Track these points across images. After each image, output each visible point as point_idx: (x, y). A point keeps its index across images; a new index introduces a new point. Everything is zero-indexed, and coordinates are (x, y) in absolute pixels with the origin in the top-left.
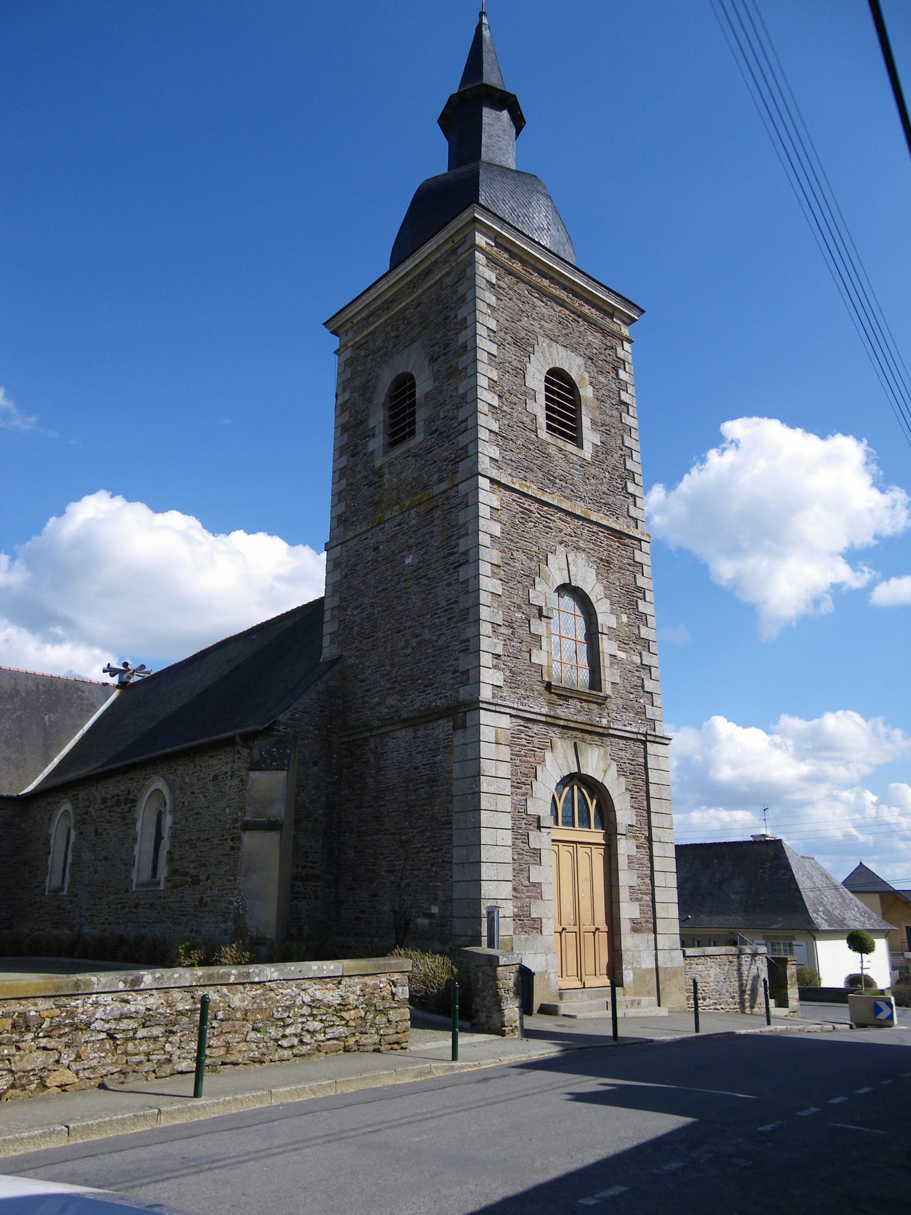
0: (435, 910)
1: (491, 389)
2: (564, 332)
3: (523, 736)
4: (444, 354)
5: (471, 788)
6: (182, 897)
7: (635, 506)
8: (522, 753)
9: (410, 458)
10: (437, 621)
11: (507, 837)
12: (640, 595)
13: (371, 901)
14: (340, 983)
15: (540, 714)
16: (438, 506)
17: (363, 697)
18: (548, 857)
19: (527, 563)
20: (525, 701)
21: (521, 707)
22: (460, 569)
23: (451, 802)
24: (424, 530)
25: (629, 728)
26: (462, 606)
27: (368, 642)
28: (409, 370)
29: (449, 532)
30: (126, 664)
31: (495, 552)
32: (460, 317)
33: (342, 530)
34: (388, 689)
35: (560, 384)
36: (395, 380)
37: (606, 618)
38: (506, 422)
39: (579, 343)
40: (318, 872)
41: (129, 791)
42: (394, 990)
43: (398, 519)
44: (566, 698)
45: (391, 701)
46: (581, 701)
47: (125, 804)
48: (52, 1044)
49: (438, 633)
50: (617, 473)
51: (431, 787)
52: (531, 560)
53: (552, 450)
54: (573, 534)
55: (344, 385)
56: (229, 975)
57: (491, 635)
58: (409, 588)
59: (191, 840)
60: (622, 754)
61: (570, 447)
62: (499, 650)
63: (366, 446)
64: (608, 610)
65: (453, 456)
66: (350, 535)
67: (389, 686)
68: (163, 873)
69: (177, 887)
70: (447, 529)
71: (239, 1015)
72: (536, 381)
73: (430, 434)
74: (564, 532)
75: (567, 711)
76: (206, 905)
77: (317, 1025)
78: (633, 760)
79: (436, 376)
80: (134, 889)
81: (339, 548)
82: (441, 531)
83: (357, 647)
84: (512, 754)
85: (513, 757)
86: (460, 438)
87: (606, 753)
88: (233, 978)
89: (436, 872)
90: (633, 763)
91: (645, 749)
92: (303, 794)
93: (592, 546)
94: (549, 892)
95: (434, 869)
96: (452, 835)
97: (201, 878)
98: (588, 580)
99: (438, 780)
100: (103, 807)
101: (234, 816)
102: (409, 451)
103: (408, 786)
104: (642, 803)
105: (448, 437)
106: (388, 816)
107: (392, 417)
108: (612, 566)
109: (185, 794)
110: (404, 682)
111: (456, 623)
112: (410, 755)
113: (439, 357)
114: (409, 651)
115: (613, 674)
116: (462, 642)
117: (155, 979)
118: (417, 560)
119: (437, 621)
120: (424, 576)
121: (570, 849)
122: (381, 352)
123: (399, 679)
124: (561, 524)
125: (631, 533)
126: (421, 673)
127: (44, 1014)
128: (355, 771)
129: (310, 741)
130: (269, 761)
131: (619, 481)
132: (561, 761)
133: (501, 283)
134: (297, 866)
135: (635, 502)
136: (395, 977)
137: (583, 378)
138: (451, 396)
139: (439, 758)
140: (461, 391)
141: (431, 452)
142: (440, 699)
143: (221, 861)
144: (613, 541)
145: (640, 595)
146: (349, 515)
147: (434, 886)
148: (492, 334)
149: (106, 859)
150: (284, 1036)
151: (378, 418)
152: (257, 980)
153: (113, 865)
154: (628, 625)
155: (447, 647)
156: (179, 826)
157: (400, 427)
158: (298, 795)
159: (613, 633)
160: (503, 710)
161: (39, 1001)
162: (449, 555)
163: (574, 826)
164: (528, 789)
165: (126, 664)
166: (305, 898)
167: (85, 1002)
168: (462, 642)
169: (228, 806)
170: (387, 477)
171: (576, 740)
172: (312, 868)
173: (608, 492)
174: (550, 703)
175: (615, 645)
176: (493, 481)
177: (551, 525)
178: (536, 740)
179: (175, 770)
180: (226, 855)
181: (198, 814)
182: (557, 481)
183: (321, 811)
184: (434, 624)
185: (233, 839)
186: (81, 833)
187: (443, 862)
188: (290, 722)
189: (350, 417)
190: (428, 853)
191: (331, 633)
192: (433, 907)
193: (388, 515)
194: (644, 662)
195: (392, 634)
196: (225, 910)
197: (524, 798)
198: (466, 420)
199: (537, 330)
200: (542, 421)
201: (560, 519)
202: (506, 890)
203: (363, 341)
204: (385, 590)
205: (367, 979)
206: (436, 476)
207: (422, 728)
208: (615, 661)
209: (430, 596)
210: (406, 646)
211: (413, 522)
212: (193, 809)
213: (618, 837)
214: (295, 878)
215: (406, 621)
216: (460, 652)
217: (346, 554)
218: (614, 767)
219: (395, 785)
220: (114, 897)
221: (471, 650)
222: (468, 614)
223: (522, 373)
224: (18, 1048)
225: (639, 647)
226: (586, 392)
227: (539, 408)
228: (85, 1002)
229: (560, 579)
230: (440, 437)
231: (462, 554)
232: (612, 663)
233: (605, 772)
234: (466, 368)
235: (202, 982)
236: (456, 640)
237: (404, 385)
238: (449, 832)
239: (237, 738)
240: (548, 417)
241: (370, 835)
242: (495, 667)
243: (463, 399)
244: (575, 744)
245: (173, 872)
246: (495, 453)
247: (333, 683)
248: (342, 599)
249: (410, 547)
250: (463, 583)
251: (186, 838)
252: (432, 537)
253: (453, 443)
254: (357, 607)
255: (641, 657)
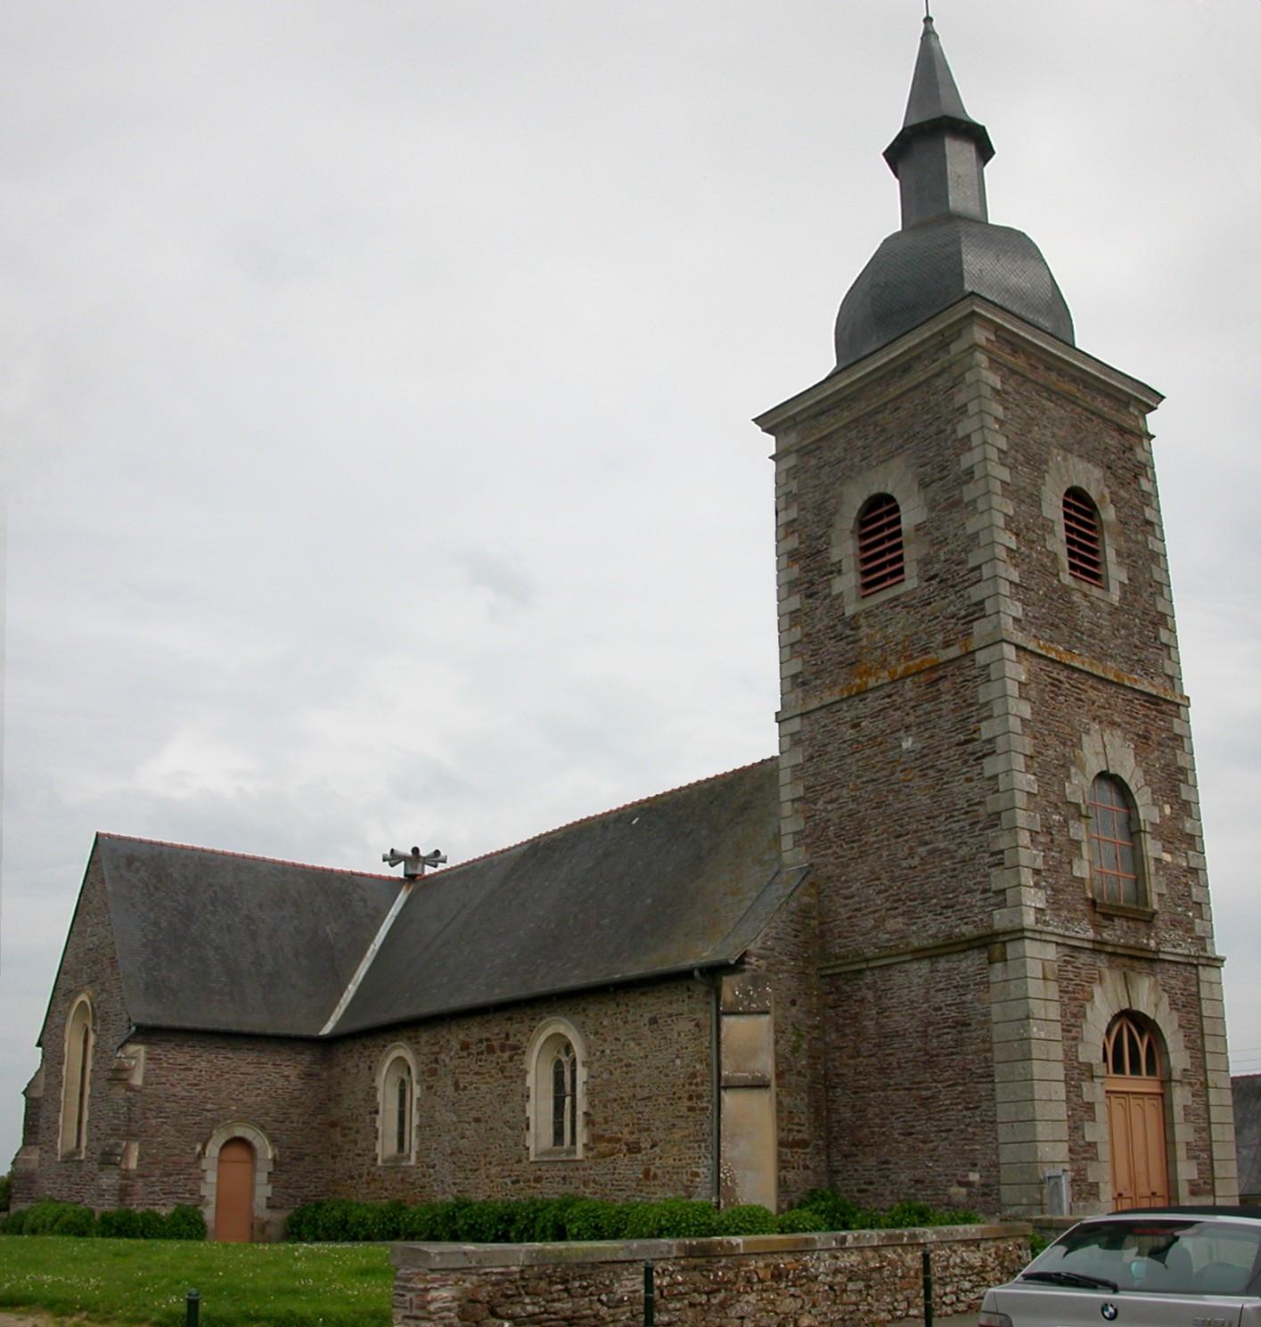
0: (974, 1177)
1: (1007, 527)
2: (1079, 437)
3: (1069, 968)
4: (941, 479)
5: (1018, 1034)
6: (615, 1168)
7: (1170, 658)
8: (1070, 989)
9: (898, 609)
10: (955, 826)
11: (1060, 1091)
12: (1181, 777)
13: (881, 1170)
14: (978, 1246)
15: (1083, 939)
16: (946, 676)
17: (850, 918)
18: (1100, 1111)
19: (1060, 748)
20: (1069, 925)
21: (1067, 933)
22: (984, 761)
23: (990, 1050)
24: (928, 707)
25: (1179, 951)
26: (990, 809)
27: (853, 848)
28: (889, 491)
29: (965, 712)
30: (415, 850)
31: (1027, 740)
32: (960, 434)
33: (800, 695)
34: (888, 910)
35: (1078, 501)
36: (866, 502)
37: (1148, 813)
38: (1025, 567)
39: (1095, 449)
40: (806, 1136)
41: (507, 1035)
42: (1020, 1253)
43: (887, 690)
44: (1109, 917)
45: (891, 924)
46: (1128, 919)
47: (503, 1051)
48: (798, 1291)
49: (959, 840)
50: (1149, 618)
51: (960, 1032)
52: (1064, 744)
53: (1076, 597)
54: (1107, 706)
55: (785, 498)
56: (902, 1236)
57: (1029, 845)
58: (910, 780)
59: (622, 1098)
60: (1172, 982)
61: (1096, 592)
62: (1039, 864)
63: (828, 584)
64: (1150, 802)
65: (963, 613)
66: (815, 704)
67: (888, 905)
68: (413, 1141)
69: (605, 1157)
70: (962, 708)
71: (912, 1273)
72: (1053, 509)
73: (927, 580)
74: (1097, 704)
75: (1114, 934)
76: (838, 1172)
77: (967, 1285)
78: (1185, 990)
79: (932, 506)
80: (532, 1159)
81: (798, 720)
82: (953, 710)
83: (835, 853)
84: (1061, 991)
85: (1062, 994)
86: (971, 590)
87: (1156, 981)
88: (905, 1239)
89: (974, 1134)
90: (1185, 993)
91: (1197, 974)
92: (782, 1042)
93: (1128, 719)
94: (1103, 1152)
95: (970, 1130)
96: (994, 1090)
97: (643, 1146)
98: (1127, 767)
99: (970, 1025)
100: (465, 1054)
101: (691, 1070)
102: (896, 598)
103: (925, 1031)
104: (1195, 1041)
105: (953, 586)
106: (900, 1068)
107: (864, 549)
108: (1150, 743)
109: (605, 1040)
110: (911, 900)
111: (983, 829)
112: (928, 992)
113: (933, 482)
114: (916, 861)
115: (1160, 883)
116: (993, 854)
117: (856, 1239)
118: (919, 746)
119: (955, 826)
120: (932, 767)
121: (1122, 1101)
122: (843, 464)
123: (903, 897)
124: (1093, 694)
125: (1168, 698)
126: (936, 890)
127: (789, 1267)
128: (845, 1011)
129: (786, 975)
130: (746, 1003)
131: (1151, 628)
132: (1110, 995)
133: (1006, 387)
134: (783, 1130)
135: (1169, 654)
136: (1021, 1240)
137: (1103, 496)
138: (956, 535)
139: (970, 997)
140: (970, 531)
141: (930, 603)
142: (966, 924)
143: (674, 1125)
144: (1149, 708)
145: (1181, 777)
146: (808, 676)
147: (972, 1150)
148: (1002, 456)
149: (477, 1120)
150: (946, 1294)
151: (845, 549)
152: (922, 1241)
153: (491, 1129)
154: (1171, 819)
155: (971, 860)
156: (598, 1081)
157: (880, 565)
158: (776, 1042)
159: (1158, 832)
160: (1048, 938)
161: (785, 1256)
162: (967, 742)
163: (1123, 1073)
164: (1078, 1032)
165: (415, 850)
166: (793, 1168)
167: (812, 1258)
168: (993, 854)
169: (678, 1057)
170: (864, 630)
171: (1125, 969)
172: (799, 1131)
173: (1141, 646)
174: (1095, 926)
175: (1159, 845)
176: (1018, 647)
177: (1083, 697)
178: (1083, 972)
179: (584, 1010)
180: (682, 1117)
181: (628, 1065)
182: (1085, 637)
183: (804, 1062)
184: (950, 829)
185: (690, 1098)
186: (429, 1088)
187: (983, 1121)
188: (762, 952)
189: (801, 543)
190: (961, 1111)
191: (795, 833)
192: (971, 1174)
193: (872, 683)
194: (1191, 865)
195: (888, 839)
196: (689, 1183)
197: (1074, 1043)
198: (979, 567)
199: (1049, 439)
200: (1064, 560)
201: (1092, 687)
202: (1062, 1151)
203: (812, 447)
204: (873, 780)
205: (998, 1243)
206: (940, 637)
207: (942, 960)
208: (1160, 865)
209: (943, 792)
210: (911, 855)
211: (910, 694)
212: (620, 1060)
213: (1173, 1084)
214: (781, 1144)
215: (909, 824)
216: (990, 867)
217: (809, 728)
218: (1166, 999)
219: (906, 1030)
220: (499, 1169)
221: (1007, 864)
222: (999, 818)
223: (1036, 501)
224: (778, 1295)
225: (1184, 846)
226: (1109, 514)
227: (1058, 543)
228: (812, 1258)
229: (1095, 766)
230: (942, 585)
231: (985, 741)
232: (1157, 870)
233: (1156, 1005)
234: (974, 501)
235: (885, 1242)
236: (984, 852)
237: (880, 509)
238: (990, 1086)
239: (696, 973)
240: (1071, 554)
241: (873, 1091)
242: (1036, 885)
243: (973, 540)
244: (1125, 974)
245: (596, 1138)
246: (1016, 609)
247: (806, 899)
248: (807, 788)
249: (908, 728)
250: (990, 779)
251: (612, 1096)
252: (940, 717)
253: (962, 596)
254: (832, 801)
255: (1187, 857)
